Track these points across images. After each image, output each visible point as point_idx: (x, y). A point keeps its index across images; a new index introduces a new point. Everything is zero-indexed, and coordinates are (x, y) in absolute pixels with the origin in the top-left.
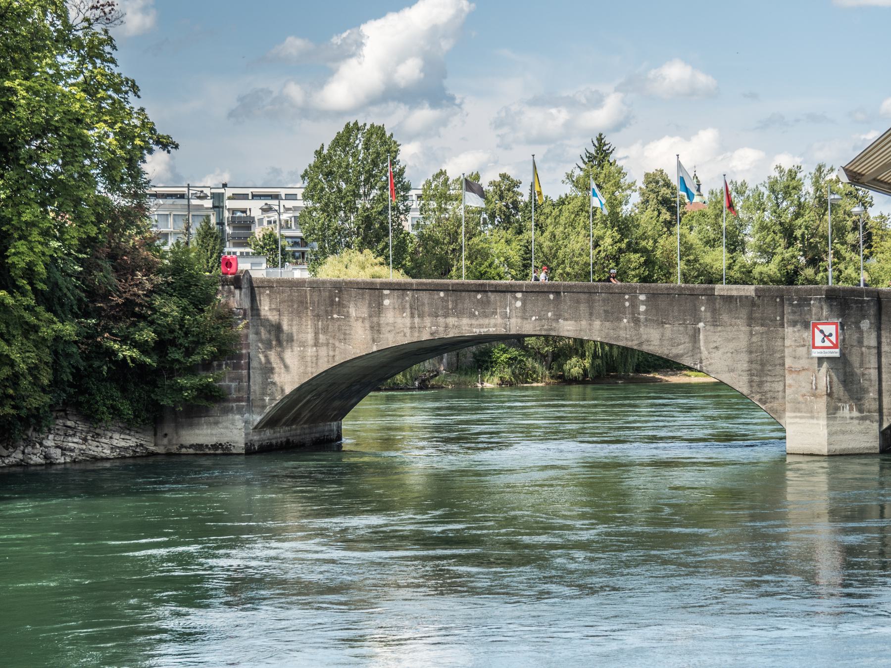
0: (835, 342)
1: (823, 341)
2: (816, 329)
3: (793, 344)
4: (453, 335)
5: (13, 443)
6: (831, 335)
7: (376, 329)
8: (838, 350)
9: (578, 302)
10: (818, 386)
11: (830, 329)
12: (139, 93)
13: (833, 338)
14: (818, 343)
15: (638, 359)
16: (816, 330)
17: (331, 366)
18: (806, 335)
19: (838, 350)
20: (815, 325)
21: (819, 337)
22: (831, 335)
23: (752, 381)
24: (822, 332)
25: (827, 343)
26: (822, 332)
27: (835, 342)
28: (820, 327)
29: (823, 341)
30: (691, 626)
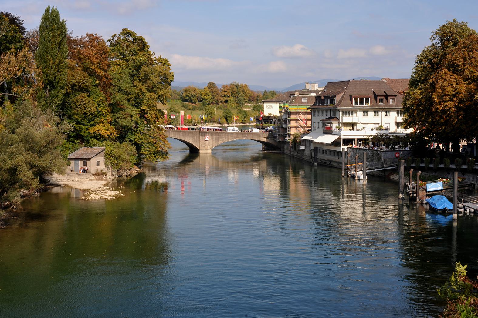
11: (208, 137)
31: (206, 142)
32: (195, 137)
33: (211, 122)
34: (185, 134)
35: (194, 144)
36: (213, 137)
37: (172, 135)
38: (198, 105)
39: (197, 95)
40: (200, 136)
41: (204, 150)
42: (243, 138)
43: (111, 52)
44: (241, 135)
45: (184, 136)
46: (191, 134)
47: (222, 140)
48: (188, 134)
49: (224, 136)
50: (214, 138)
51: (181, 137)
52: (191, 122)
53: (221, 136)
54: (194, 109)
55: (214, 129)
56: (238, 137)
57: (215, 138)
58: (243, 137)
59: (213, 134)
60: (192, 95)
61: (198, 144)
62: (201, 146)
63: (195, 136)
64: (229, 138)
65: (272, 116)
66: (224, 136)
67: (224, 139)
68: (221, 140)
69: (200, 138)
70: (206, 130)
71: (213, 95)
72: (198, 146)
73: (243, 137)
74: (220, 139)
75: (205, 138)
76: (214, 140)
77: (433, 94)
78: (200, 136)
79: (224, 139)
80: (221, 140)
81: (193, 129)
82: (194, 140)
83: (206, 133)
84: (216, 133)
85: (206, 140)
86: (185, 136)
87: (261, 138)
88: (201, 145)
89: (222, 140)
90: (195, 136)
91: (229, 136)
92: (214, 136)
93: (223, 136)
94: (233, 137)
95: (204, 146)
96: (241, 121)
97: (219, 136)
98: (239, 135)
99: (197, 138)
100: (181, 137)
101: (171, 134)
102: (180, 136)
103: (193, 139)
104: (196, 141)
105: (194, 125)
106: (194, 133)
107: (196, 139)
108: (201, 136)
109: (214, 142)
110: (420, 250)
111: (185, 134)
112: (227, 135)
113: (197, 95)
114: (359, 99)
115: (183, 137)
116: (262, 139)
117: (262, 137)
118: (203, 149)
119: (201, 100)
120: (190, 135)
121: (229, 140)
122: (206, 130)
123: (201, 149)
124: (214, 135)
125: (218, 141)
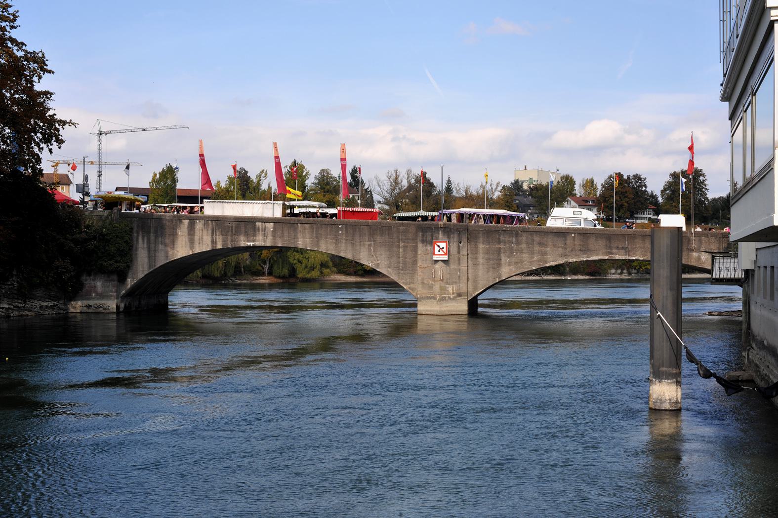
0: (445, 252)
1: (439, 251)
2: (435, 245)
3: (422, 253)
4: (179, 257)
5: (63, 125)
6: (443, 248)
7: (192, 242)
8: (447, 256)
9: (305, 229)
10: (436, 276)
11: (443, 245)
12: (49, 68)
13: (445, 250)
14: (436, 252)
15: (15, 290)
16: (435, 245)
17: (166, 262)
18: (429, 248)
19: (447, 256)
20: (435, 243)
21: (437, 249)
22: (443, 248)
23: (400, 273)
24: (439, 246)
25: (441, 252)
26: (439, 246)
27: (445, 252)
28: (438, 244)
29: (439, 251)
30: (242, 376)
31: (437, 266)
32: (399, 247)
36: (476, 247)
37: (304, 237)
40: (420, 245)
42: (22, 316)
46: (382, 236)
47: (516, 263)
48: (372, 235)
49: (524, 246)
50: (481, 251)
51: (343, 246)
53: (511, 242)
56: (586, 250)
57: (487, 252)
58: (610, 248)
59: (476, 237)
63: (402, 244)
64: (544, 254)
66: (524, 246)
67: (525, 256)
68: (514, 260)
69: (419, 252)
70: (454, 220)
73: (610, 248)
74: (504, 259)
76: (481, 260)
77: (623, 273)
78: (420, 245)
79: (525, 256)
80: (514, 260)
82: (394, 259)
84: (488, 233)
85: (435, 258)
86: (357, 238)
87: (695, 254)
88: (423, 279)
89: (516, 263)
90: (402, 244)
91: (546, 246)
92: (481, 246)
97: (502, 246)
99: (410, 254)
100: (343, 246)
101: (300, 235)
102: (337, 241)
103: (390, 257)
104: (405, 263)
106: (394, 230)
108: (423, 241)
109: (481, 271)
112: (537, 238)
114: (684, 276)
115: (350, 248)
116: (699, 258)
117: (699, 251)
118: (428, 298)
120: (379, 239)
121: (546, 262)
122: (454, 220)
124: (481, 239)
125: (499, 265)
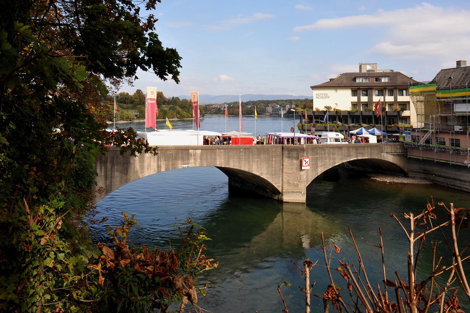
1: (305, 164)
6: (307, 162)
8: (309, 167)
11: (307, 160)
13: (308, 163)
24: (305, 161)
25: (307, 165)
26: (305, 161)
33: (142, 118)
34: (251, 155)
35: (270, 180)
37: (220, 159)
38: (130, 105)
39: (129, 99)
41: (294, 194)
43: (126, 244)
44: (354, 151)
45: (249, 162)
46: (264, 154)
47: (324, 165)
49: (327, 155)
52: (127, 118)
53: (322, 154)
54: (127, 108)
55: (305, 138)
60: (125, 98)
61: (279, 180)
62: (288, 183)
63: (274, 159)
65: (332, 110)
66: (327, 155)
71: (140, 99)
72: (279, 183)
74: (319, 163)
75: (301, 162)
81: (130, 123)
83: (303, 150)
86: (251, 157)
93: (325, 154)
94: (342, 155)
95: (298, 185)
96: (163, 117)
97: (318, 156)
98: (351, 150)
101: (218, 157)
105: (130, 121)
106: (270, 150)
107: (275, 167)
110: (382, 237)
111: (251, 155)
113: (129, 99)
118: (293, 192)
119: (132, 102)
120: (262, 156)
121: (335, 163)
123: (288, 192)
125: (317, 167)
